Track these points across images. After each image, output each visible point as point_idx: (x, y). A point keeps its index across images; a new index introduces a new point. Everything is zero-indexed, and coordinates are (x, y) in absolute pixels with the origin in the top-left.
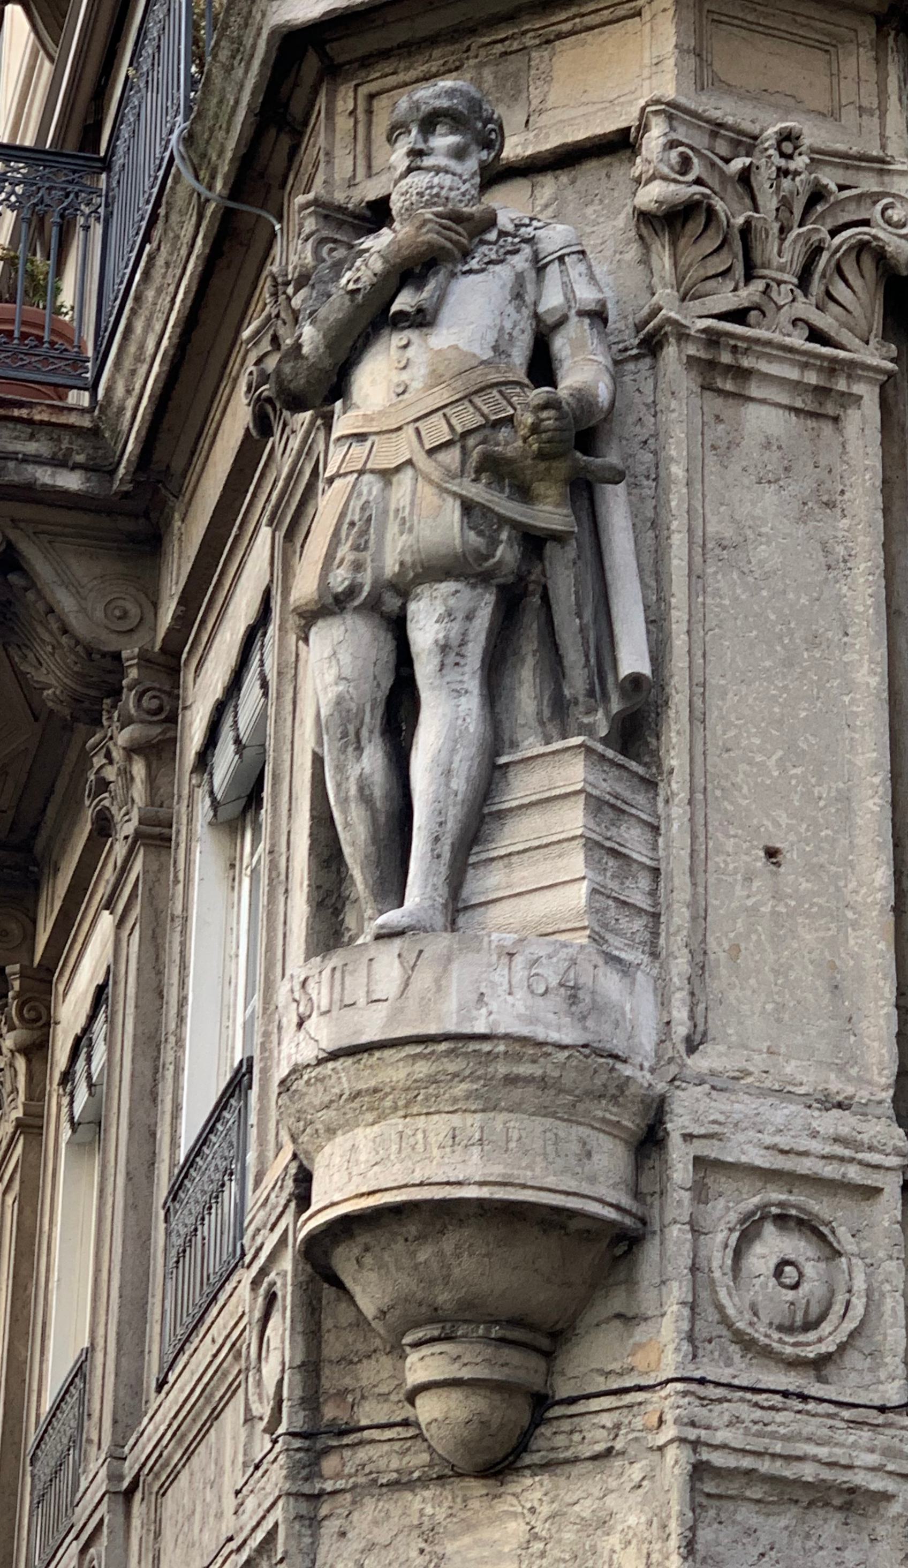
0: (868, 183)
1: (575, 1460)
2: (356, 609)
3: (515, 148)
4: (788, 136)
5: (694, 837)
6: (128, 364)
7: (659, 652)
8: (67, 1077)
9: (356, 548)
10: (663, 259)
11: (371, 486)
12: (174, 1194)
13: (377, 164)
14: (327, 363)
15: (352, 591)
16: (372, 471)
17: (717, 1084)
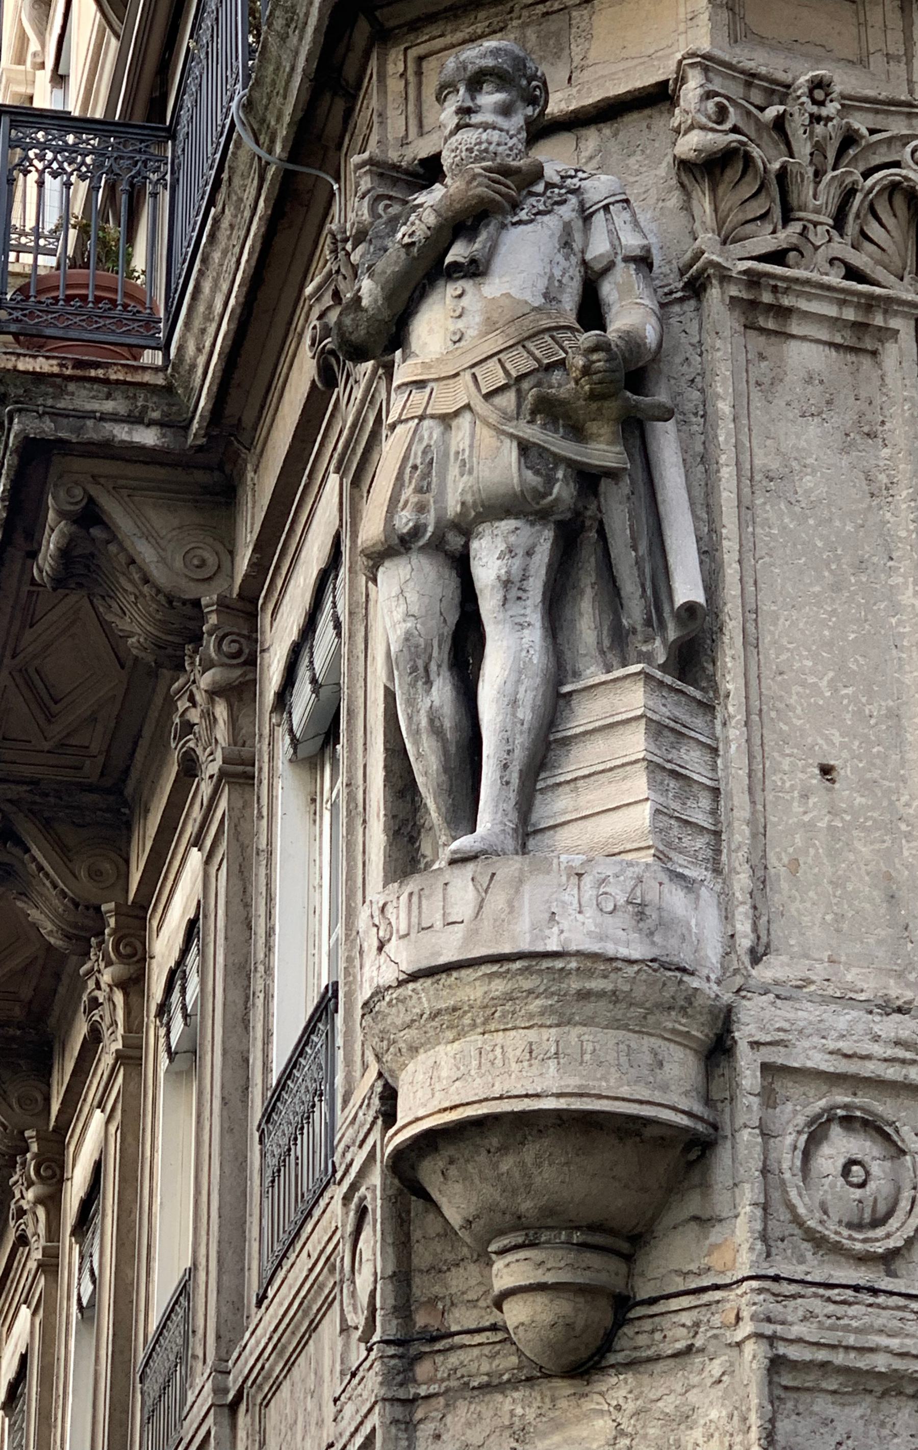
1: (658, 1358)
2: (422, 549)
3: (559, 103)
4: (818, 84)
5: (751, 757)
6: (197, 323)
7: (712, 582)
8: (163, 1009)
9: (419, 490)
11: (431, 431)
12: (268, 1116)
14: (386, 314)
15: (417, 531)
16: (432, 417)
17: (783, 994)
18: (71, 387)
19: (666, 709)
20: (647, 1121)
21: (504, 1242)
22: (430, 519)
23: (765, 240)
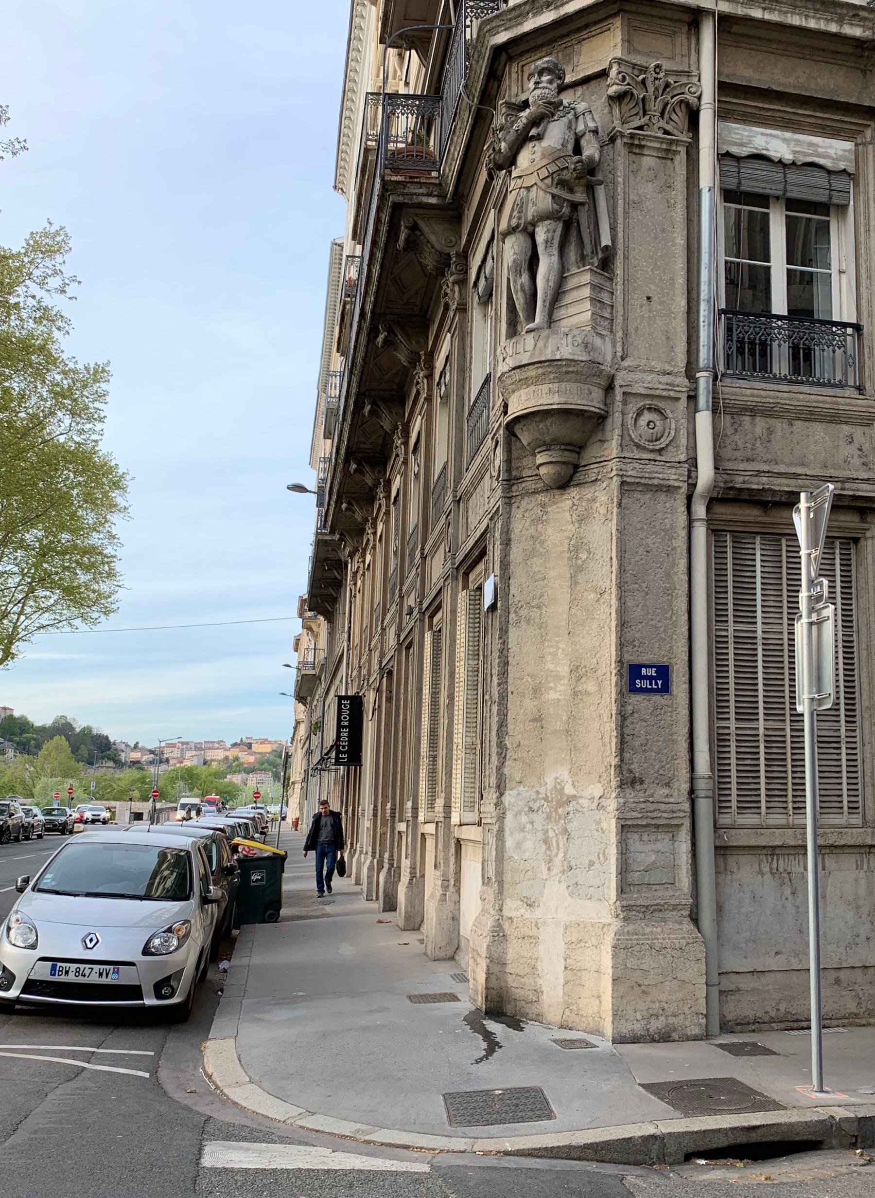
0: (684, 80)
1: (586, 483)
3: (568, 79)
4: (658, 66)
5: (624, 295)
6: (449, 161)
7: (614, 239)
8: (439, 384)
9: (519, 212)
10: (616, 111)
11: (523, 192)
12: (470, 415)
13: (525, 88)
14: (510, 154)
15: (518, 226)
17: (630, 369)
18: (409, 185)
19: (597, 280)
20: (586, 411)
21: (540, 449)
22: (523, 221)
23: (637, 123)
